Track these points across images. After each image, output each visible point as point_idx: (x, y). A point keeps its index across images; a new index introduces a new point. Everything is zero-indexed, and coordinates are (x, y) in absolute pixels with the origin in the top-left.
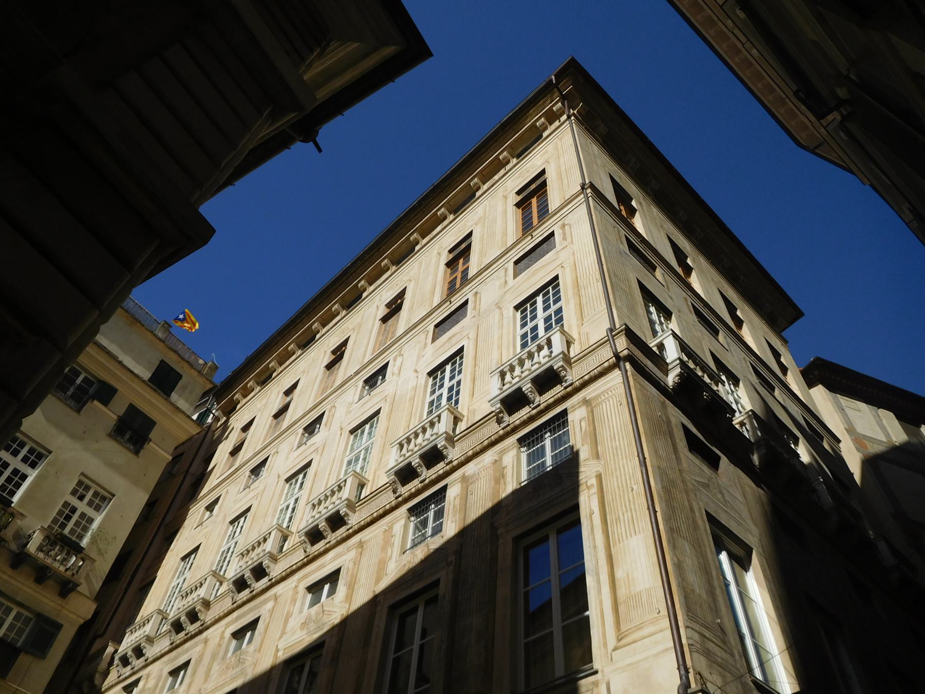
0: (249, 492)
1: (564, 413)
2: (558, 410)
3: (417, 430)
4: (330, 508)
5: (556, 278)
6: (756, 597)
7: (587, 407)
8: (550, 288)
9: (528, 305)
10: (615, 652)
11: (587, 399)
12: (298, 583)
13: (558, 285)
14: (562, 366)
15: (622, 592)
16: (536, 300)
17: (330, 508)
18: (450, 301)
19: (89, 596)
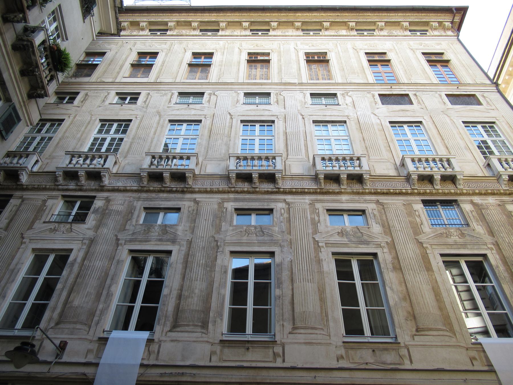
0: (185, 109)
1: (94, 197)
2: (93, 194)
3: (443, 158)
4: (427, 169)
5: (130, 121)
6: (182, 332)
7: (106, 203)
8: (124, 123)
9: (124, 123)
10: (290, 335)
11: (24, 197)
12: (48, 199)
13: (61, 124)
14: (191, 176)
15: (297, 309)
16: (113, 124)
17: (427, 169)
18: (458, 88)
19: (60, 83)
